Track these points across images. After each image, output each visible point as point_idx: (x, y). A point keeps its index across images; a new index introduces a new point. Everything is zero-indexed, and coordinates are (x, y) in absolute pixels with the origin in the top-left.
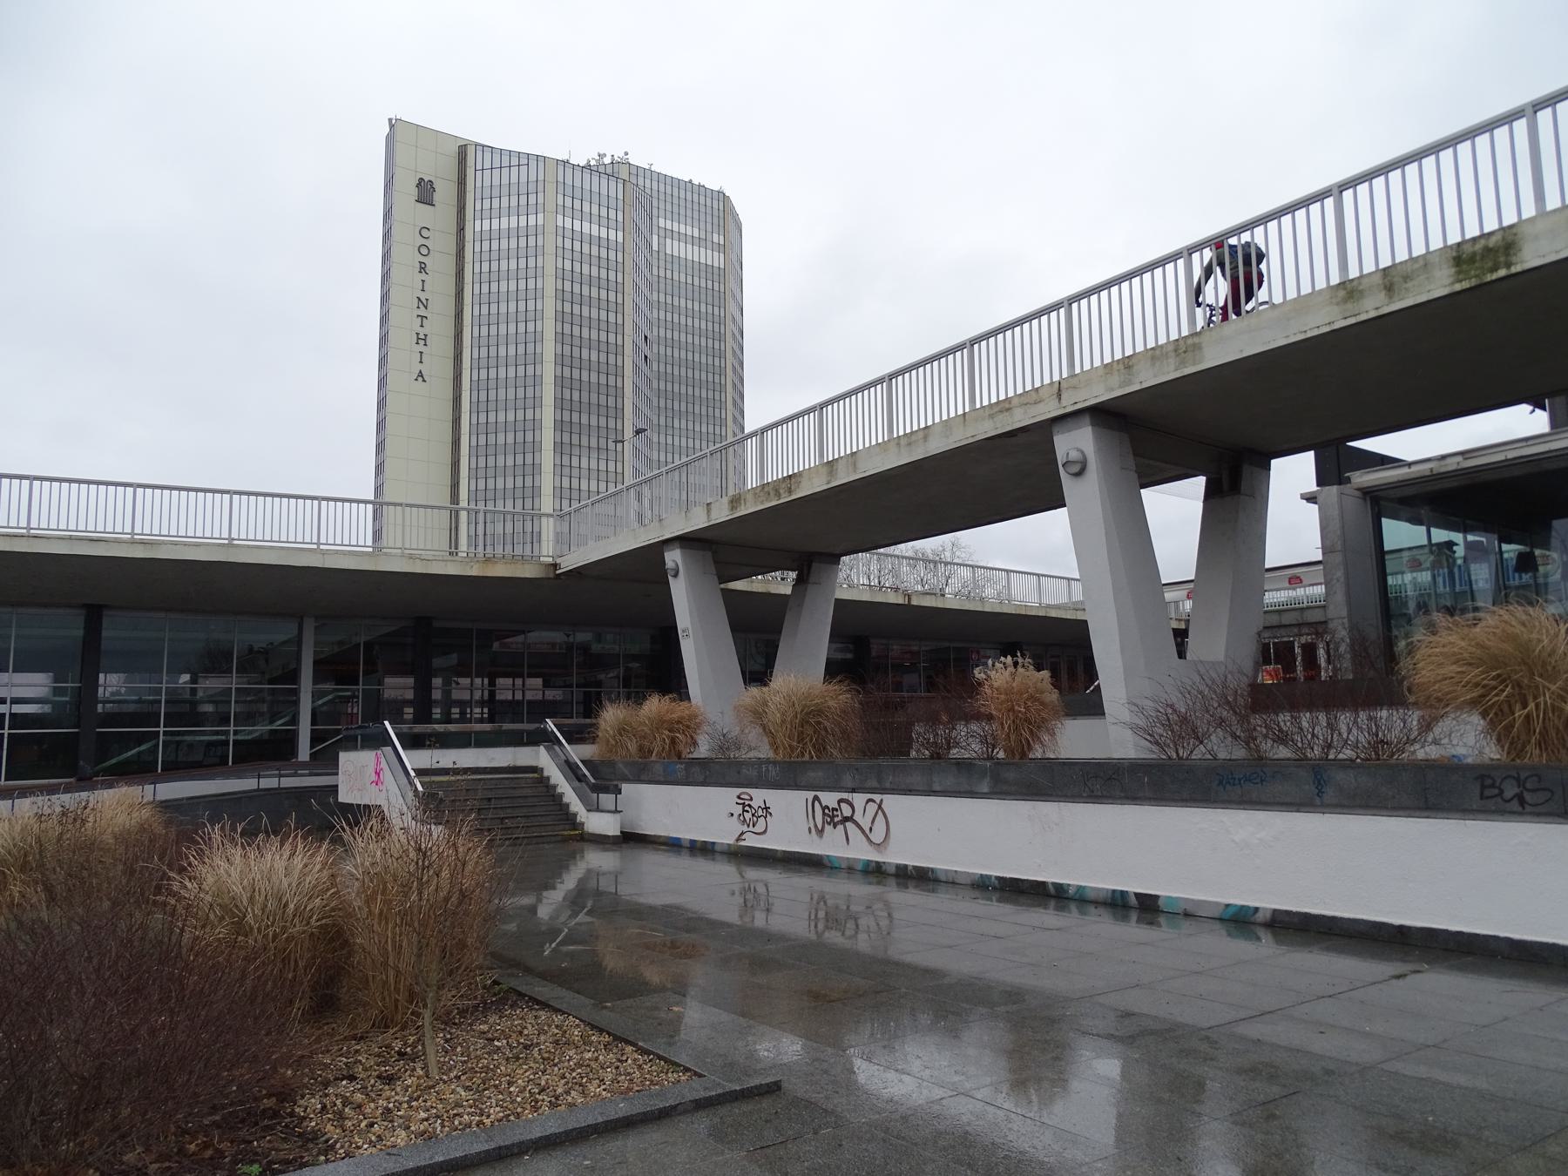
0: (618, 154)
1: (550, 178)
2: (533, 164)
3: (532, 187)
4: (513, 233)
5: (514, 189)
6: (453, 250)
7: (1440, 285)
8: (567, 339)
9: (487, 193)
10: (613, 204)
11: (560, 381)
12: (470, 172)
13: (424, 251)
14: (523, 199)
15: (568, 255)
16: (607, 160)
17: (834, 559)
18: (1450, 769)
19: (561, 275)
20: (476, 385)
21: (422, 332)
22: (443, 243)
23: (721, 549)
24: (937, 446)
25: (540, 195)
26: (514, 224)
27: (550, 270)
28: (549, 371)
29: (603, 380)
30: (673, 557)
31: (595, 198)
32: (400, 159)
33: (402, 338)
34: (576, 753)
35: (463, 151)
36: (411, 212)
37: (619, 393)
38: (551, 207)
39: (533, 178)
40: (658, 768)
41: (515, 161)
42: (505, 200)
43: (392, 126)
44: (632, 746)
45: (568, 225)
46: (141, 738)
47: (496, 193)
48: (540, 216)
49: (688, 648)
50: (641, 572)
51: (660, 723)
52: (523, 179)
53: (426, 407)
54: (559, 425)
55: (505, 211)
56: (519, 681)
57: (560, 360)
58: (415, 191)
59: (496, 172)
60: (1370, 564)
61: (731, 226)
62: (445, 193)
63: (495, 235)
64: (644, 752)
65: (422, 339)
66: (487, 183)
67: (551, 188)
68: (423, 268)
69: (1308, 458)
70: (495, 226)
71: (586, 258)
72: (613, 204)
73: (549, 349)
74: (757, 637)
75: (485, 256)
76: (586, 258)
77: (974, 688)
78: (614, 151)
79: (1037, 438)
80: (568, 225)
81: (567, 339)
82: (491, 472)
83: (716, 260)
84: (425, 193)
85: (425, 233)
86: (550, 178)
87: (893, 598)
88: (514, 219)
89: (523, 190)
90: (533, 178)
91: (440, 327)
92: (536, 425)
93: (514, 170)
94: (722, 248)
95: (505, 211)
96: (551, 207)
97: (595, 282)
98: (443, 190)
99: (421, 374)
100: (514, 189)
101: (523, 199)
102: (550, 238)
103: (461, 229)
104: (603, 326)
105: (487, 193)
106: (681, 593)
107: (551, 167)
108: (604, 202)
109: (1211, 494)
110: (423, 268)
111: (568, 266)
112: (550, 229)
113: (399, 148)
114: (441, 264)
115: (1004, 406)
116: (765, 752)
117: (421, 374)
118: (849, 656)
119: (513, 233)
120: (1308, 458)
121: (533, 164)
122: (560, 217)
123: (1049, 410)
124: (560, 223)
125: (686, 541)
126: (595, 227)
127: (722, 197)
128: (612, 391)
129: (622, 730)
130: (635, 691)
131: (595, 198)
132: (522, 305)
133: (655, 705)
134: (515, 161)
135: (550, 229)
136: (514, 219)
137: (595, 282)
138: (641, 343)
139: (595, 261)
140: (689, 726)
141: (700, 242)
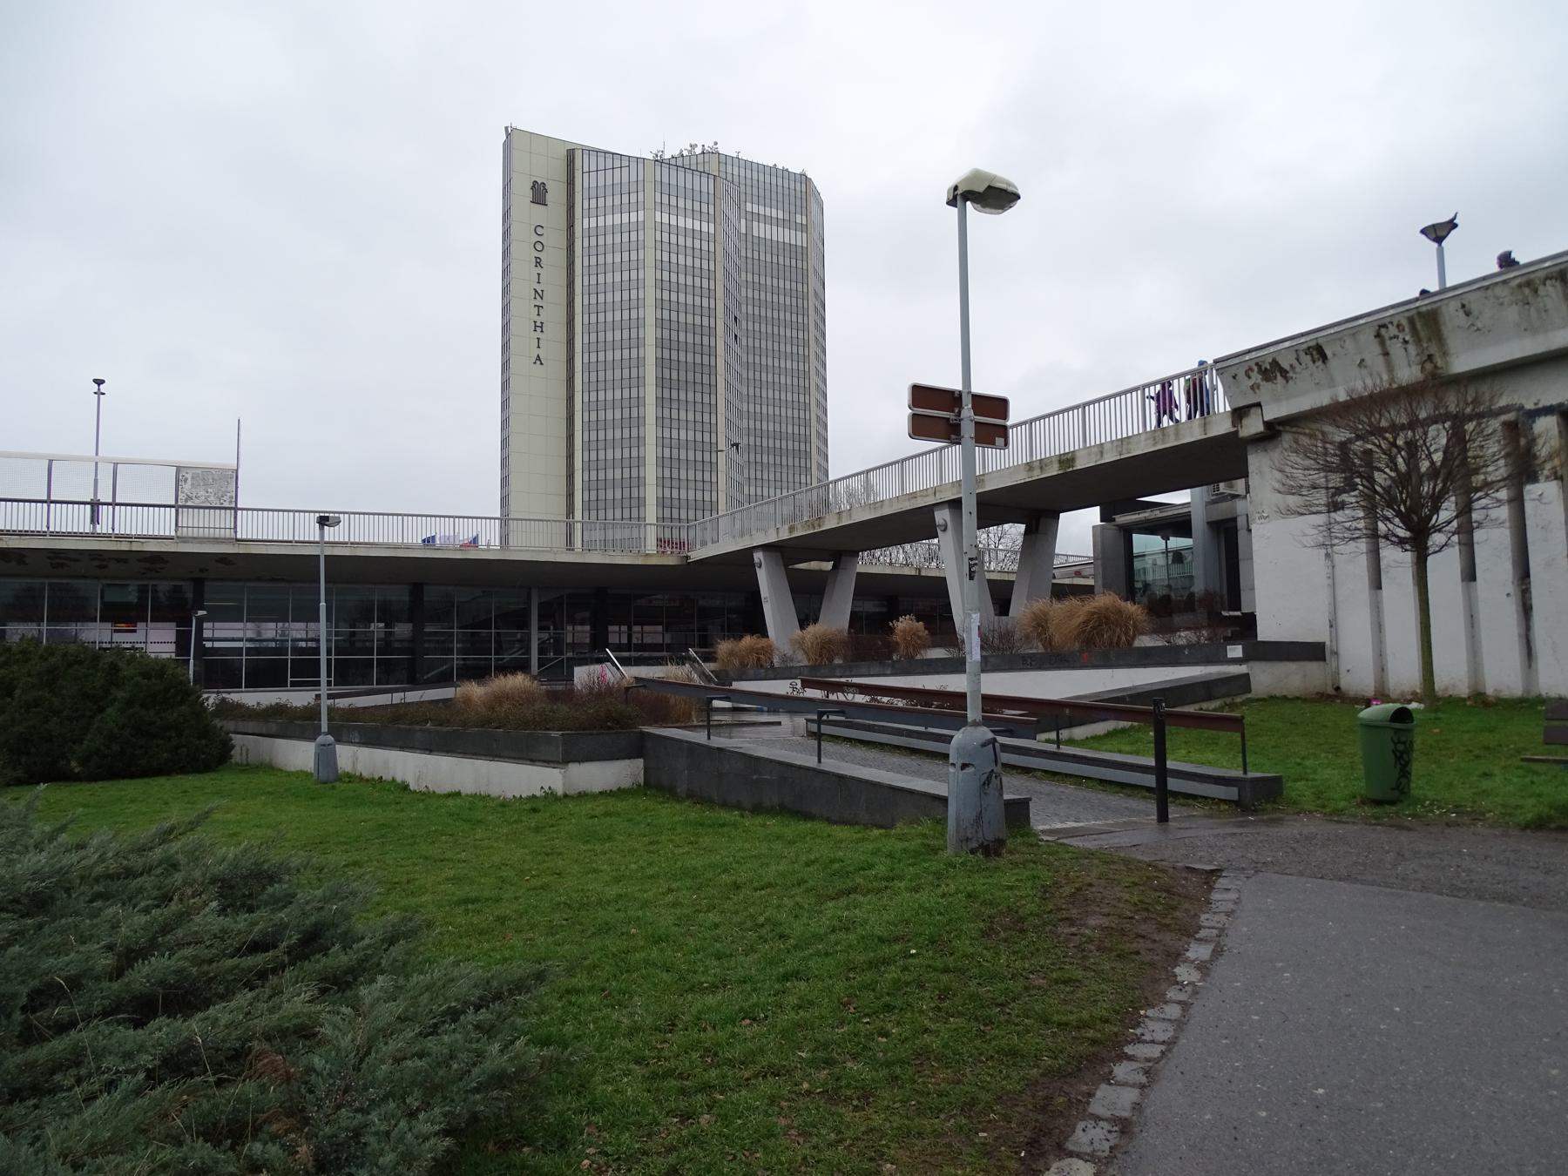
0: (709, 144)
1: (649, 177)
2: (633, 165)
3: (633, 188)
4: (617, 229)
5: (617, 189)
6: (564, 244)
7: (1054, 471)
8: (666, 324)
9: (593, 194)
10: (705, 199)
11: (660, 362)
12: (578, 174)
13: (539, 247)
14: (625, 198)
15: (666, 247)
16: (698, 151)
17: (854, 554)
18: (1031, 656)
19: (660, 265)
20: (587, 367)
21: (539, 320)
22: (555, 239)
23: (784, 552)
24: (887, 511)
25: (641, 194)
26: (617, 221)
27: (650, 262)
28: (650, 354)
29: (698, 360)
30: (758, 556)
31: (689, 194)
32: (517, 164)
33: (522, 327)
34: (708, 667)
35: (571, 155)
36: (526, 211)
37: (712, 370)
38: (650, 204)
39: (633, 178)
40: (751, 672)
41: (617, 164)
42: (609, 200)
43: (508, 135)
44: (736, 662)
45: (665, 220)
46: (445, 661)
47: (601, 193)
48: (641, 213)
49: (767, 609)
50: (741, 562)
51: (752, 650)
52: (625, 180)
53: (544, 386)
54: (660, 401)
55: (609, 210)
56: (624, 628)
57: (660, 344)
58: (529, 193)
59: (601, 167)
60: (1122, 563)
61: (814, 207)
62: (556, 194)
63: (601, 231)
64: (743, 665)
65: (539, 327)
66: (593, 184)
67: (649, 187)
68: (538, 262)
69: (1097, 509)
70: (601, 223)
71: (682, 250)
72: (705, 199)
73: (650, 334)
74: (808, 598)
75: (593, 251)
76: (682, 250)
77: (891, 630)
78: (704, 141)
79: (929, 510)
80: (665, 220)
81: (666, 324)
82: (601, 445)
83: (797, 238)
84: (539, 194)
85: (539, 231)
86: (649, 177)
87: (907, 571)
88: (617, 216)
89: (625, 190)
90: (633, 178)
91: (554, 315)
92: (640, 402)
93: (617, 171)
94: (804, 228)
95: (609, 210)
96: (650, 204)
97: (690, 271)
98: (556, 190)
99: (538, 358)
100: (617, 189)
101: (625, 198)
102: (650, 232)
103: (571, 226)
104: (698, 310)
105: (593, 194)
106: (762, 576)
107: (649, 166)
108: (697, 197)
109: (1027, 532)
110: (538, 262)
111: (666, 277)
112: (650, 224)
113: (516, 155)
114: (554, 258)
115: (913, 496)
116: (805, 663)
117: (538, 358)
118: (884, 610)
119: (617, 229)
120: (1097, 509)
121: (633, 165)
122: (658, 214)
123: (931, 501)
124: (658, 219)
125: (766, 548)
126: (689, 221)
127: (804, 179)
128: (706, 370)
129: (732, 653)
130: (735, 632)
131: (689, 194)
132: (626, 294)
133: (748, 640)
134: (617, 164)
135: (650, 224)
136: (617, 216)
137: (690, 271)
138: (732, 324)
139: (689, 252)
140: (768, 651)
141: (783, 223)
